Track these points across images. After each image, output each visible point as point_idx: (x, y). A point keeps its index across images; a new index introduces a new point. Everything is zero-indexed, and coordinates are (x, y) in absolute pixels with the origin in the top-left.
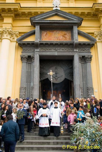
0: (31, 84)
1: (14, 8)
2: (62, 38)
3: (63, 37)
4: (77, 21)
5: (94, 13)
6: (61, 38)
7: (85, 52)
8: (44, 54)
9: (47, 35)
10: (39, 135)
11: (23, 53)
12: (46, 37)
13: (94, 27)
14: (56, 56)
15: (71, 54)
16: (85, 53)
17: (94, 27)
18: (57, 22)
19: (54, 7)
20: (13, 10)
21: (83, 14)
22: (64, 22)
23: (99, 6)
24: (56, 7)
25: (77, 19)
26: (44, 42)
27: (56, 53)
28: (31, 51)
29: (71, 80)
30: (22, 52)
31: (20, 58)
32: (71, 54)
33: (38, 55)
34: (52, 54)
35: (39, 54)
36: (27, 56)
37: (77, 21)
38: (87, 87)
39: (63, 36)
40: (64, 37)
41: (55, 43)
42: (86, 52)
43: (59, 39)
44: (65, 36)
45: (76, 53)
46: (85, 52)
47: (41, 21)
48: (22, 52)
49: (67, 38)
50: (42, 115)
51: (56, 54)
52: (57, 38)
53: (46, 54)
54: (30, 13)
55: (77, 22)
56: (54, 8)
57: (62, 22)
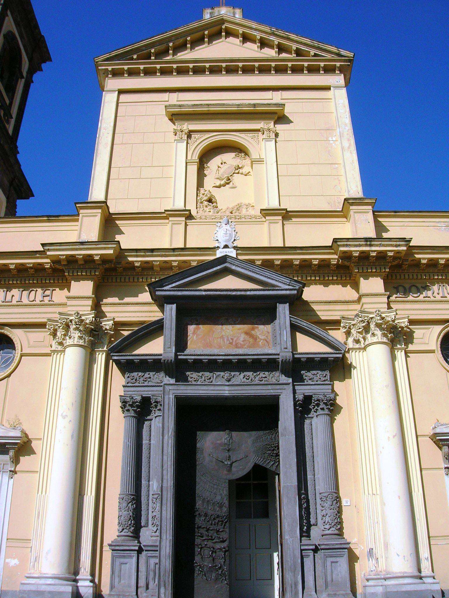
0: (153, 485)
1: (102, 255)
2: (243, 341)
3: (247, 337)
4: (286, 290)
5: (338, 261)
6: (242, 339)
7: (312, 385)
8: (191, 392)
9: (198, 332)
10: (203, 450)
11: (127, 389)
12: (195, 337)
13: (155, 580)
14: (226, 398)
15: (272, 391)
16: (312, 387)
17: (155, 580)
18: (229, 293)
19: (218, 247)
20: (97, 260)
21: (306, 265)
22: (248, 293)
23: (349, 245)
24: (226, 247)
25: (289, 285)
26: (190, 355)
27: (226, 388)
28: (150, 384)
29: (273, 469)
30: (124, 386)
31: (120, 404)
32: (272, 391)
33: (172, 397)
34: (213, 392)
35: (175, 392)
36: (139, 398)
37: (286, 290)
38: (320, 492)
39: (246, 333)
40: (252, 336)
41: (224, 357)
42: (315, 385)
43: (234, 343)
44: (253, 332)
45: (285, 386)
46: (312, 385)
47: (179, 293)
48: (124, 386)
49: (258, 340)
50: (239, 207)
51: (227, 392)
52: (228, 340)
53: (196, 392)
54: (147, 267)
55: (288, 292)
56: (220, 250)
57: (243, 293)
